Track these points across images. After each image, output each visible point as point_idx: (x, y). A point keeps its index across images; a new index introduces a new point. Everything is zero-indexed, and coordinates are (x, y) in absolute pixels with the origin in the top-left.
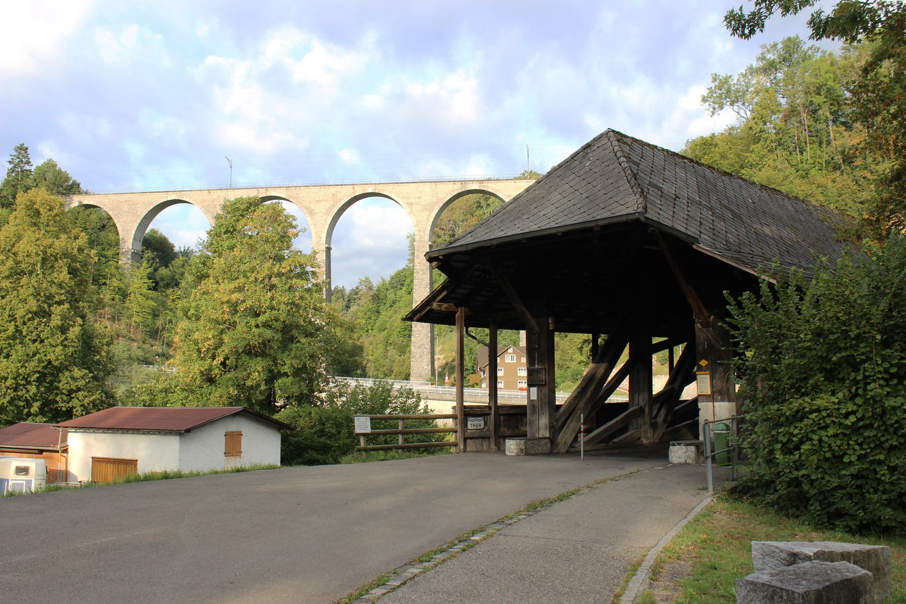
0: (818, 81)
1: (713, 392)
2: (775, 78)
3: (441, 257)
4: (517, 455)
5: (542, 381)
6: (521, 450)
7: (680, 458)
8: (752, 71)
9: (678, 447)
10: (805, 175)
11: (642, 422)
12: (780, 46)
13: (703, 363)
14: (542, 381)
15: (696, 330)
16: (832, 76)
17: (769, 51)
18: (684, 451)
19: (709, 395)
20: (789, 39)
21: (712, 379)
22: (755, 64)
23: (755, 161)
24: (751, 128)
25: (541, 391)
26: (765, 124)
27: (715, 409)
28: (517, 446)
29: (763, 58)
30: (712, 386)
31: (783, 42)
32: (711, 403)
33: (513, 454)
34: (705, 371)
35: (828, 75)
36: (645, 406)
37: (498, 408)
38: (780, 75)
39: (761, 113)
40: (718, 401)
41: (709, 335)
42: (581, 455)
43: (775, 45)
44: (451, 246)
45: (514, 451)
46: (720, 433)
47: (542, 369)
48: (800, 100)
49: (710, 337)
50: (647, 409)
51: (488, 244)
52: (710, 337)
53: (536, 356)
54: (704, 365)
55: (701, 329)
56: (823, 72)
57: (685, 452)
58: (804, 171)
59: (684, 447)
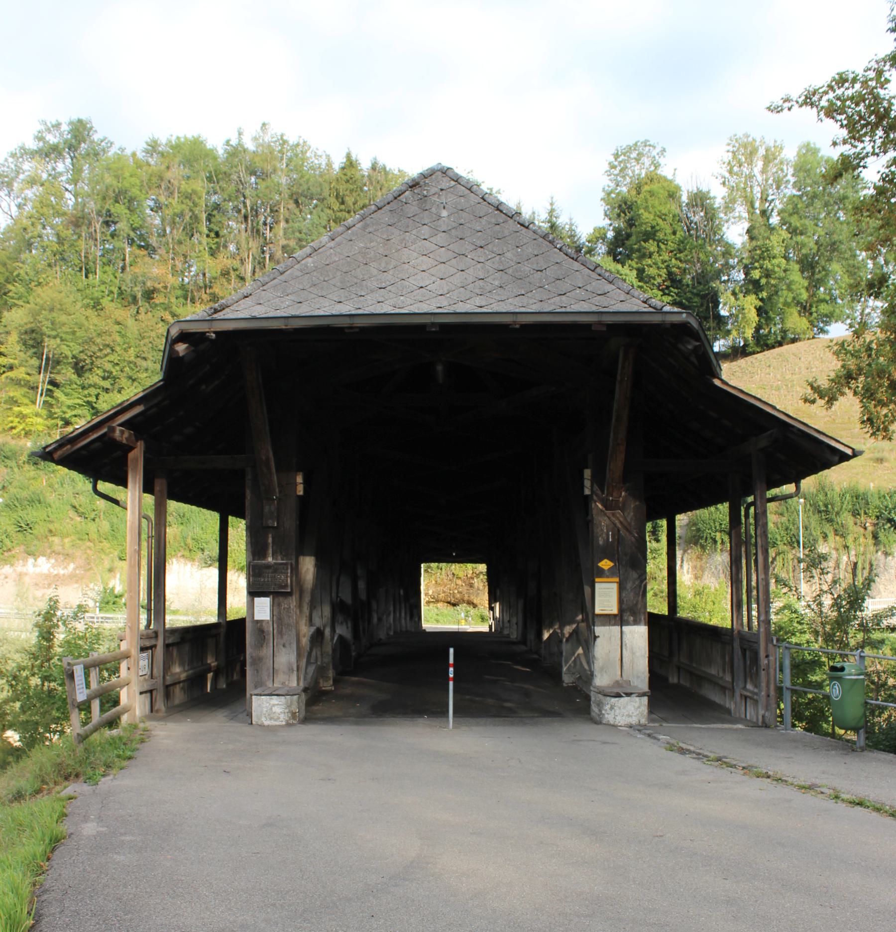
0: (120, 185)
1: (621, 610)
2: (54, 169)
3: (214, 335)
4: (288, 725)
5: (286, 586)
6: (294, 715)
7: (629, 716)
8: (25, 153)
9: (627, 699)
10: (96, 305)
11: (319, 653)
12: (65, 128)
13: (606, 564)
14: (286, 586)
15: (594, 512)
16: (138, 182)
17: (50, 132)
18: (637, 705)
19: (615, 615)
20: (80, 121)
21: (621, 588)
22: (33, 145)
23: (28, 275)
24: (25, 229)
25: (279, 605)
26: (44, 228)
27: (624, 636)
28: (289, 706)
29: (40, 138)
30: (621, 601)
31: (71, 123)
32: (618, 628)
33: (280, 723)
34: (608, 577)
35: (133, 180)
36: (324, 627)
37: (165, 631)
38: (60, 167)
39: (41, 211)
40: (628, 624)
41: (617, 522)
42: (448, 717)
43: (57, 126)
44: (215, 316)
45: (282, 716)
46: (857, 679)
47: (286, 564)
48: (92, 206)
49: (619, 525)
50: (327, 632)
51: (345, 322)
52: (619, 525)
53: (270, 540)
54: (606, 568)
55: (602, 511)
56: (127, 174)
57: (639, 707)
58: (92, 299)
59: (637, 699)
